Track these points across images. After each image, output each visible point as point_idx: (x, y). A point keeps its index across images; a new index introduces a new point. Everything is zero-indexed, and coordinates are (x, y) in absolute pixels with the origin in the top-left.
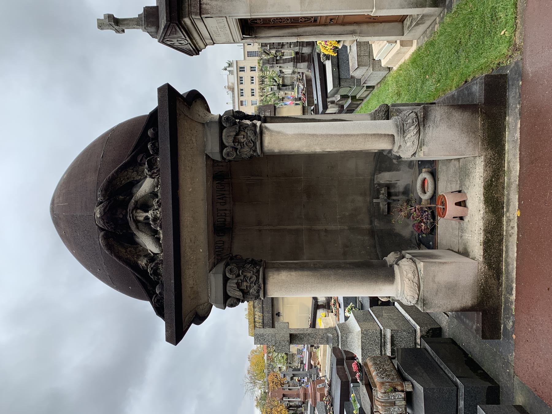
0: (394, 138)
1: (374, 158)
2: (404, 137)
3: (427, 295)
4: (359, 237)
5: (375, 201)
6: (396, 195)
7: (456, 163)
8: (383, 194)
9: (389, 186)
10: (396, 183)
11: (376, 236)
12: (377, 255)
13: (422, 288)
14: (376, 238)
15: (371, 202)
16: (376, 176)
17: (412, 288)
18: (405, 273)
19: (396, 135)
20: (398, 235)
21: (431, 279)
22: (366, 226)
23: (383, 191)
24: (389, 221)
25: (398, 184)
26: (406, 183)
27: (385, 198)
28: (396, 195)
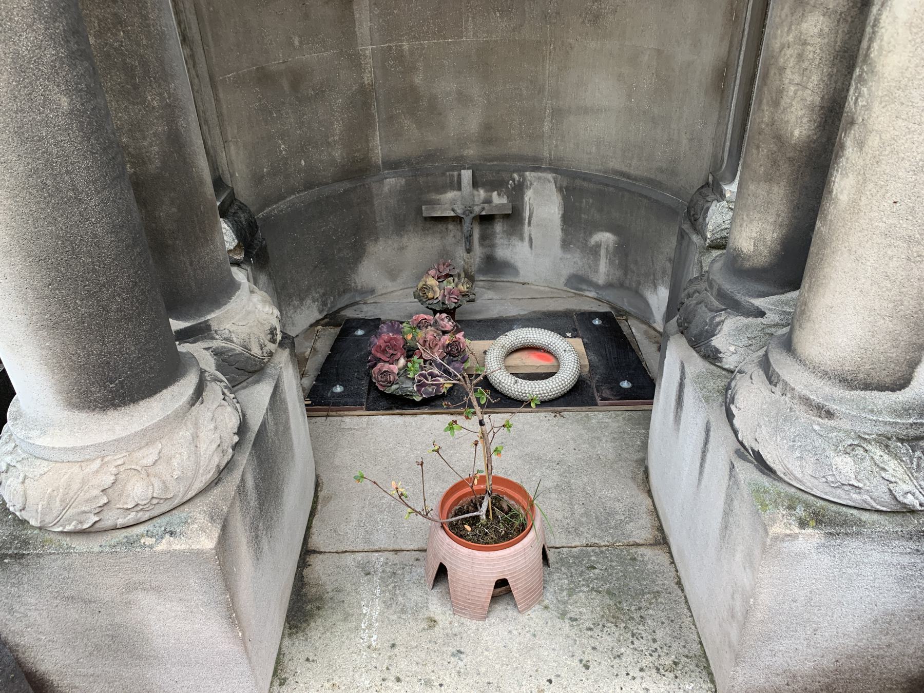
0: (881, 388)
1: (616, 172)
2: (884, 441)
3: (53, 566)
4: (337, 128)
5: (467, 175)
6: (483, 238)
7: (641, 531)
8: (488, 201)
9: (513, 218)
10: (522, 239)
11: (347, 185)
12: (281, 198)
13: (80, 545)
14: (341, 187)
15: (460, 163)
16: (550, 176)
17: (66, 506)
18: (149, 456)
19: (902, 396)
20: (358, 253)
21: (136, 578)
22: (379, 148)
23: (499, 200)
24: (400, 226)
25: (520, 244)
26: (519, 264)
27: (477, 210)
28: (485, 238)
